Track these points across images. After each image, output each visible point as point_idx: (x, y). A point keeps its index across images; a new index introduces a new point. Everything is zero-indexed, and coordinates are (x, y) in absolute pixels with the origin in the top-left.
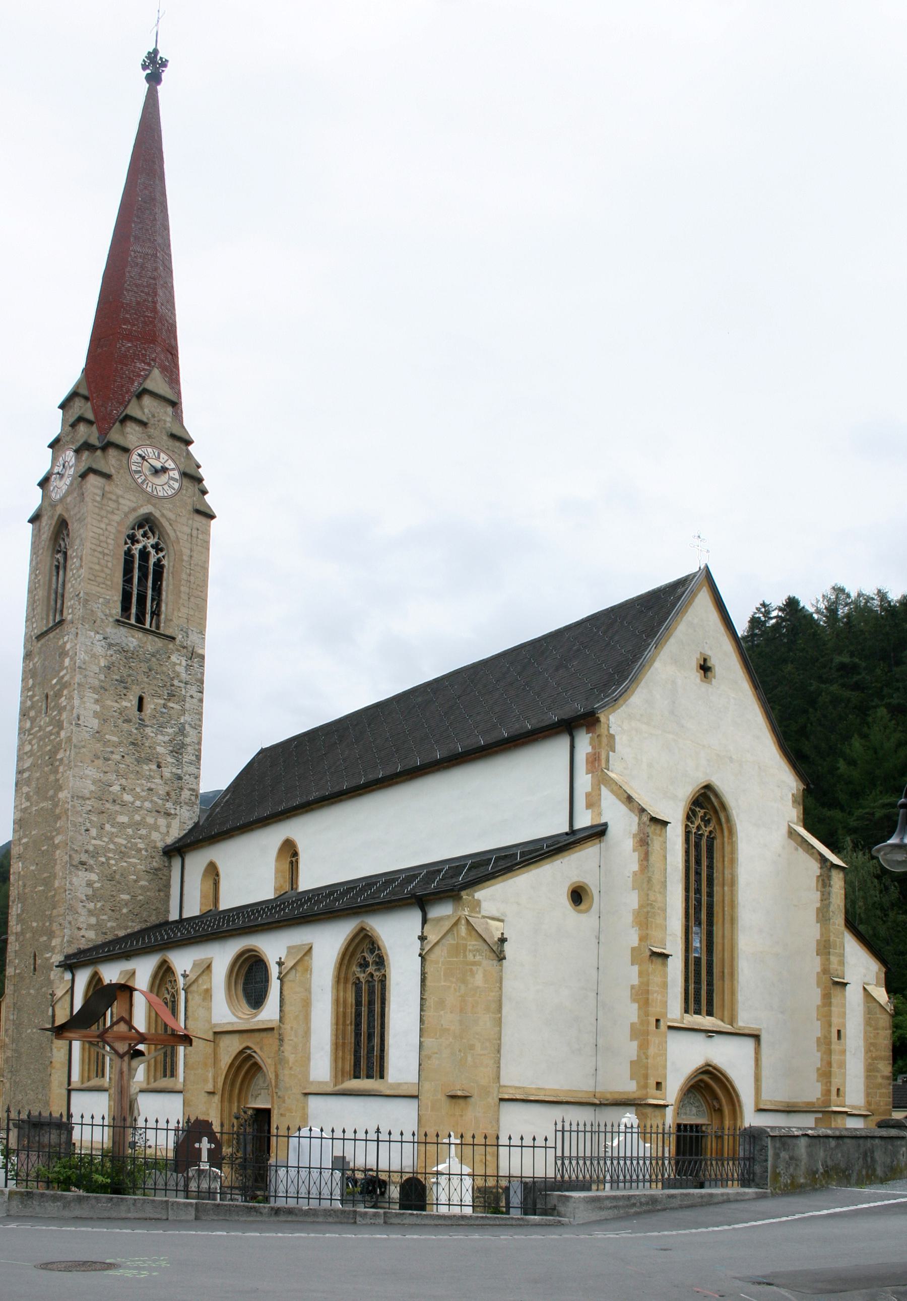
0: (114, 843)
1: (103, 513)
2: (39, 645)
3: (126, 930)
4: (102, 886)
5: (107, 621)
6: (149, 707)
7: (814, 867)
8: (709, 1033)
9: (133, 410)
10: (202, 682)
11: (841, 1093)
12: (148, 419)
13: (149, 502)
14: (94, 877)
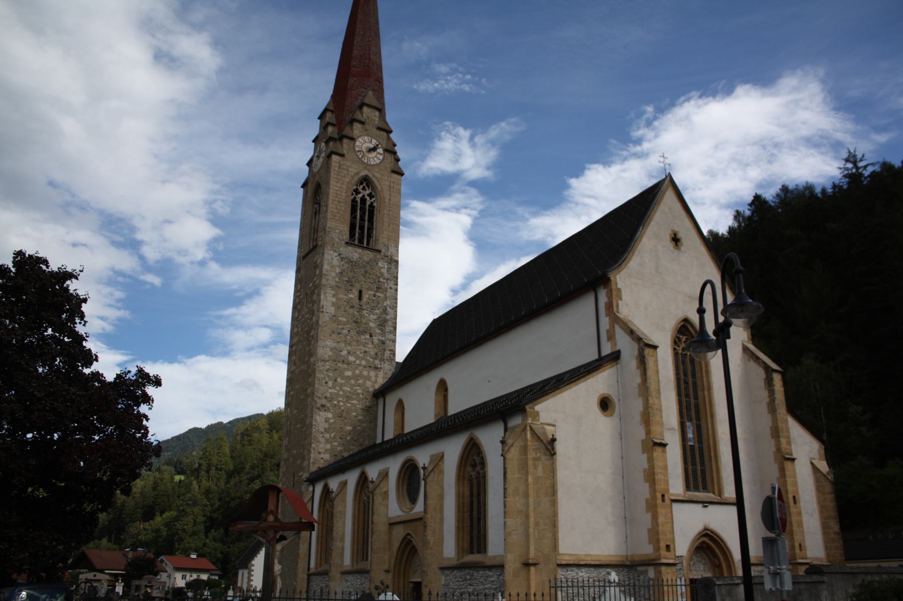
0: (343, 391)
1: (339, 177)
2: (304, 263)
3: (349, 452)
4: (335, 421)
5: (340, 244)
6: (365, 297)
7: (761, 373)
8: (705, 503)
9: (358, 115)
10: (397, 278)
11: (802, 547)
12: (365, 119)
13: (365, 168)
14: (330, 415)
